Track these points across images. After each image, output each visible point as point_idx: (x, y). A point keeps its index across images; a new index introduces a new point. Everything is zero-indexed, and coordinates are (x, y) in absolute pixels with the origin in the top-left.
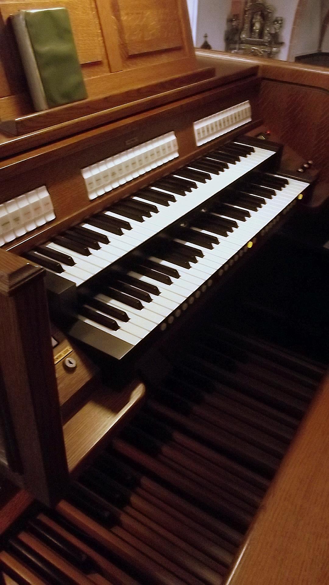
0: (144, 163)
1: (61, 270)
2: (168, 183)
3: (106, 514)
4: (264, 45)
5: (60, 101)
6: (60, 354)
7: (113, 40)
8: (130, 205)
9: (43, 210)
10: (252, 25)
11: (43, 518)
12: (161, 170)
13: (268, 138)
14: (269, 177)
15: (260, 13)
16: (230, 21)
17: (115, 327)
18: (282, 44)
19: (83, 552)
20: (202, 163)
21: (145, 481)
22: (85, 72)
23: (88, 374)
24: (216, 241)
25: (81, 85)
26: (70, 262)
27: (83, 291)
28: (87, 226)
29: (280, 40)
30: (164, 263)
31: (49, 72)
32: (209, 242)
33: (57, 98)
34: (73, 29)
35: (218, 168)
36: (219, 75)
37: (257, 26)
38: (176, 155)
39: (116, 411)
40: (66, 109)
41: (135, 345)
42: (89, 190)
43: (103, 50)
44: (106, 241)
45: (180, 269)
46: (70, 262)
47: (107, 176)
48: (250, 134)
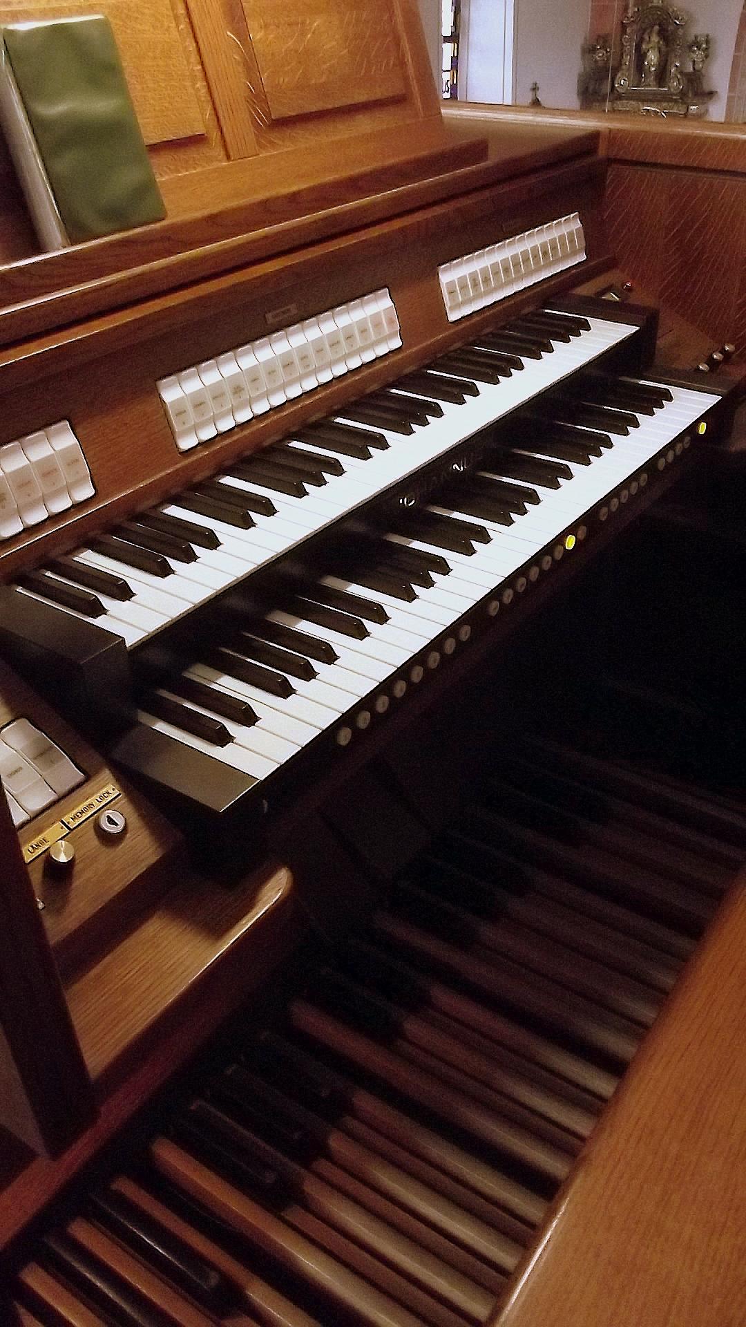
0: (314, 362)
1: (99, 610)
2: (376, 407)
3: (270, 1178)
4: (671, 100)
5: (95, 224)
6: (88, 802)
7: (233, 85)
8: (282, 460)
9: (64, 477)
10: (641, 56)
11: (126, 1187)
12: (357, 378)
13: (626, 299)
14: (624, 384)
15: (657, 28)
16: (589, 50)
17: (223, 738)
18: (711, 94)
19: (213, 1266)
20: (464, 361)
21: (365, 1102)
22: (164, 159)
23: (154, 848)
24: (484, 537)
25: (147, 188)
26: (123, 592)
27: (158, 657)
28: (174, 511)
29: (707, 88)
30: (355, 589)
31: (65, 163)
32: (465, 540)
33: (90, 218)
34: (127, 64)
35: (496, 370)
36: (493, 159)
37: (653, 57)
38: (396, 343)
39: (217, 932)
40: (111, 245)
41: (262, 779)
42: (177, 428)
43: (209, 110)
44: (212, 542)
45: (389, 603)
46: (123, 592)
47: (223, 394)
48: (585, 290)
